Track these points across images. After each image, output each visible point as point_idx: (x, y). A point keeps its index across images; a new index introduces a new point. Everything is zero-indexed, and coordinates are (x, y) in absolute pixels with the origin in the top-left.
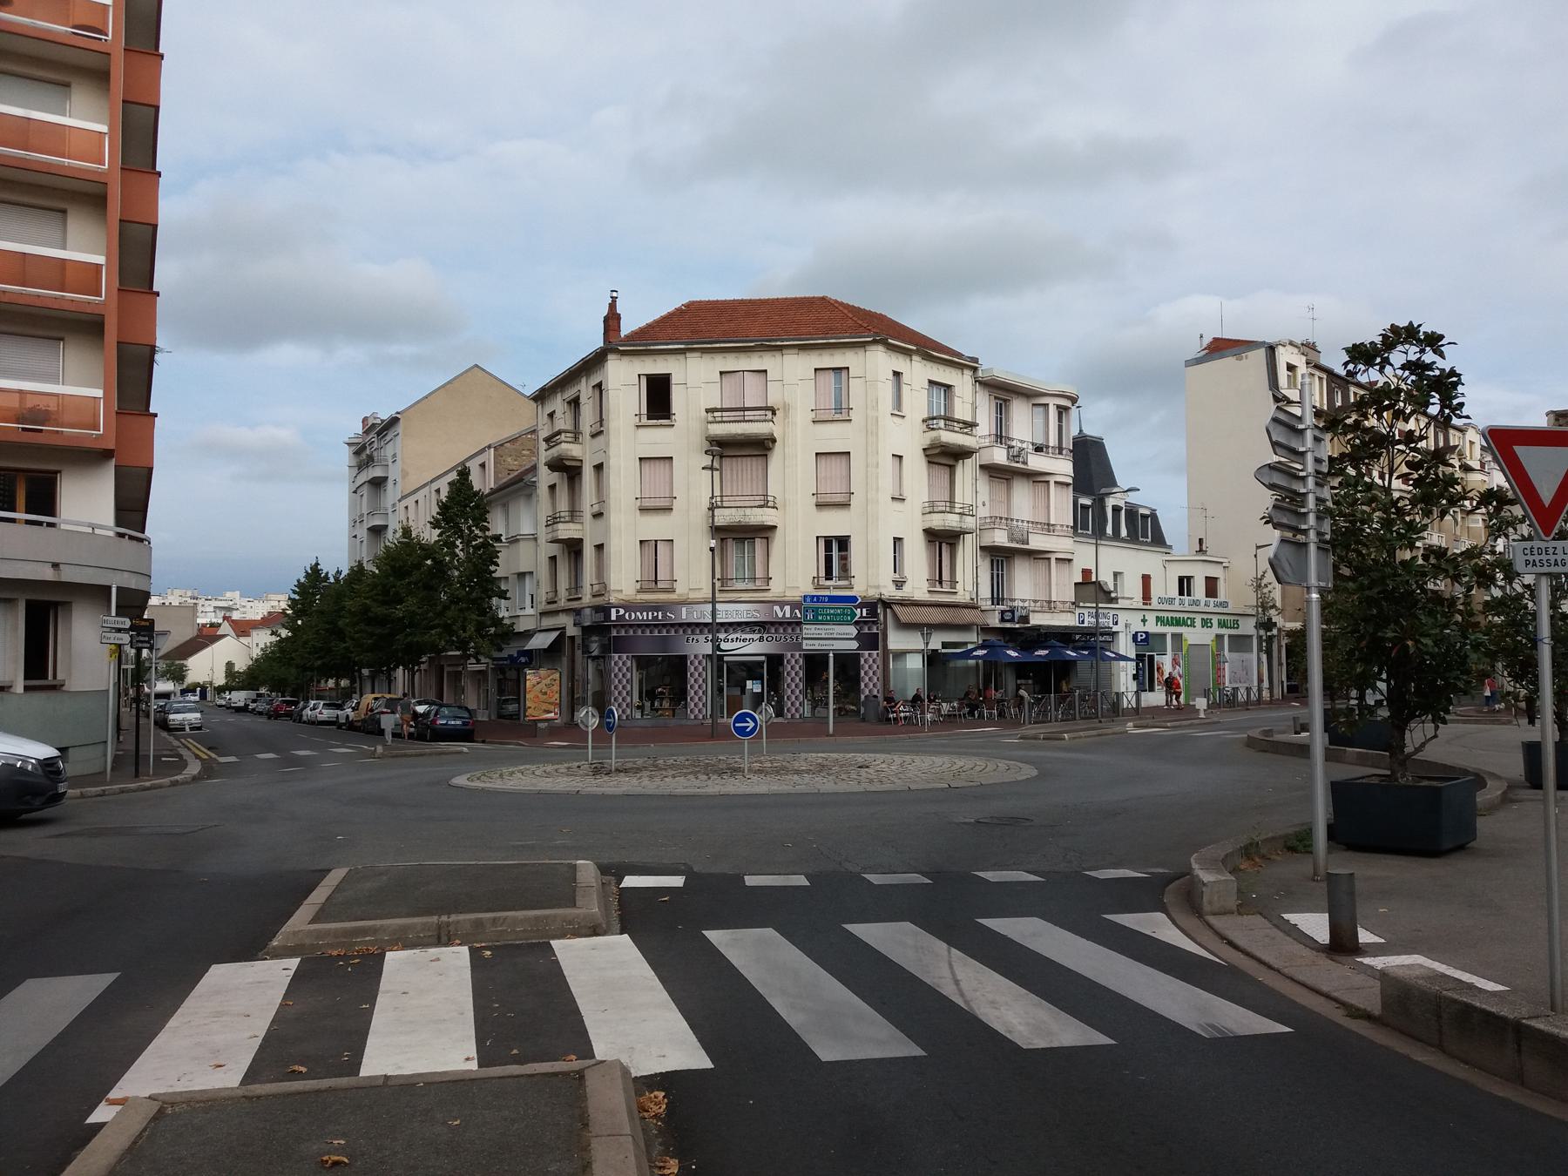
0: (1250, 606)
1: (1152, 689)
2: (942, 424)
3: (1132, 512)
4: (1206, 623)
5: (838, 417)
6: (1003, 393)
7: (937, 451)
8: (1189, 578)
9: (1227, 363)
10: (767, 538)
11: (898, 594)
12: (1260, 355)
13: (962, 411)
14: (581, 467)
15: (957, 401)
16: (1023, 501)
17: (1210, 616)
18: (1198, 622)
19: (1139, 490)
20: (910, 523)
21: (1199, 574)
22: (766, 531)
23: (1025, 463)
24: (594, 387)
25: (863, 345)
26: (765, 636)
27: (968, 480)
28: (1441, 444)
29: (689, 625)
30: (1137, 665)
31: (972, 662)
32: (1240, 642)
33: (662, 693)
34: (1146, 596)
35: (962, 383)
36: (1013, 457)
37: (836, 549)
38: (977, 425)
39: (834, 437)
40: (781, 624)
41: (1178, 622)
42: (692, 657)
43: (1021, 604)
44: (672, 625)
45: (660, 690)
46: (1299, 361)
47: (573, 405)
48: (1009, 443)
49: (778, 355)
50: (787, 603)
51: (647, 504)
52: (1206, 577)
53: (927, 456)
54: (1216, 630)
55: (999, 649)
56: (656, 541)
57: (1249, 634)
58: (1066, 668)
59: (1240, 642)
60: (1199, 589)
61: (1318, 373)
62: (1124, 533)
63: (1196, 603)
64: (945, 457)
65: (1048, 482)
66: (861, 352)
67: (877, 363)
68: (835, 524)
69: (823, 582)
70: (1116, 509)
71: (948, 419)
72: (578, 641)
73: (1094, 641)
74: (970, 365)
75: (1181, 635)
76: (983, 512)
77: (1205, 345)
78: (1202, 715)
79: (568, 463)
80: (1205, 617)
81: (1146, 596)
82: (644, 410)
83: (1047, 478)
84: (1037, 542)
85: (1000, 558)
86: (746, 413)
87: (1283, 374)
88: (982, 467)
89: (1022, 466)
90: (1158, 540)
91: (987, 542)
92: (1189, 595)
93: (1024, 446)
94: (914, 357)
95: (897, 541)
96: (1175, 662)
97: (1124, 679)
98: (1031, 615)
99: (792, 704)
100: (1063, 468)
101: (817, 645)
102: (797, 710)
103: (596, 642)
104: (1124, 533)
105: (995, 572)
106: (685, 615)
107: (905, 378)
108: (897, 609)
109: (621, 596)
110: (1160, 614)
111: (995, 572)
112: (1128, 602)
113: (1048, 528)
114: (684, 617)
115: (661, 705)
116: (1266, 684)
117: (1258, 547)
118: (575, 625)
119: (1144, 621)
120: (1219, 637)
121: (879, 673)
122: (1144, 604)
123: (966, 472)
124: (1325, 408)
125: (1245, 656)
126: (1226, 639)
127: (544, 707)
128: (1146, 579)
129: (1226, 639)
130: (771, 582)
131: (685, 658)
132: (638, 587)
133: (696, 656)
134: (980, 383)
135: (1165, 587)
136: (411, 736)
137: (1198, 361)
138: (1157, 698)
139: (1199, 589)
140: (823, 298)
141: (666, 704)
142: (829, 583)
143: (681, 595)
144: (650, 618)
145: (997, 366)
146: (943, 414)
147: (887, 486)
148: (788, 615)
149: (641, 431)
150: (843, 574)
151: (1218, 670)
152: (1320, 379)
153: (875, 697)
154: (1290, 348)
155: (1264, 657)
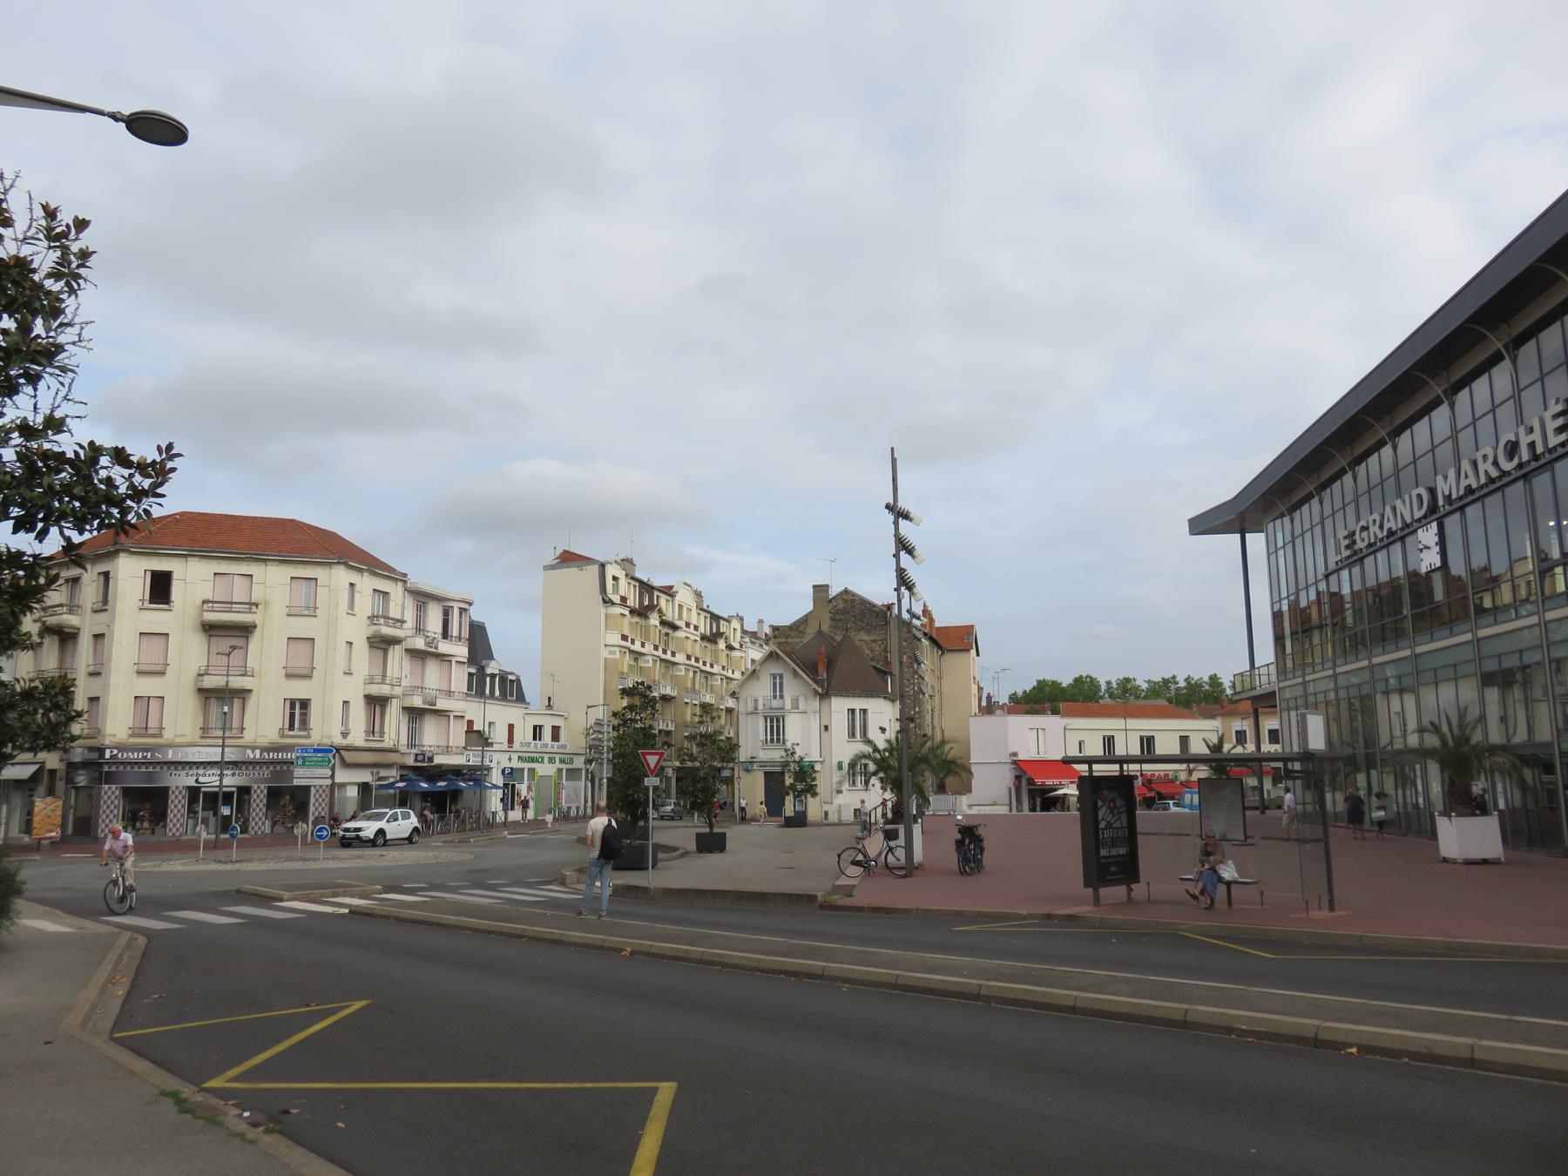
0: (582, 748)
1: (512, 809)
2: (382, 621)
3: (503, 677)
4: (551, 760)
5: (306, 612)
6: (422, 598)
7: (378, 640)
8: (541, 727)
9: (571, 572)
10: (244, 699)
11: (344, 742)
12: (596, 568)
13: (394, 612)
14: (77, 634)
15: (392, 604)
16: (433, 675)
17: (554, 755)
18: (546, 760)
19: (94, 322)
20: (355, 691)
21: (548, 724)
22: (243, 694)
23: (436, 648)
24: (99, 574)
25: (329, 564)
26: (237, 772)
27: (396, 658)
28: (714, 631)
29: (173, 763)
30: (504, 791)
31: (391, 791)
32: (573, 774)
33: (143, 816)
34: (511, 740)
35: (396, 591)
36: (428, 644)
37: (299, 709)
38: (406, 622)
39: (303, 627)
40: (251, 763)
41: (532, 760)
42: (174, 789)
43: (429, 749)
44: (158, 763)
45: (142, 813)
46: (621, 574)
47: (70, 584)
48: (426, 634)
49: (263, 565)
50: (257, 748)
51: (142, 668)
52: (553, 726)
53: (369, 642)
54: (558, 765)
55: (415, 782)
56: (149, 697)
57: (854, 867)
58: (456, 794)
59: (573, 774)
60: (547, 734)
61: (633, 582)
62: (497, 693)
63: (545, 745)
64: (381, 644)
65: (451, 661)
66: (327, 569)
67: (341, 576)
68: (299, 690)
69: (287, 732)
70: (493, 676)
71: (387, 618)
72: (61, 774)
73: (476, 775)
74: (400, 578)
75: (534, 769)
76: (405, 682)
77: (557, 555)
78: (549, 826)
79: (67, 630)
80: (551, 756)
81: (511, 740)
82: (147, 596)
83: (450, 658)
84: (442, 704)
85: (415, 715)
86: (234, 606)
87: (610, 583)
88: (406, 650)
89: (435, 651)
90: (521, 699)
91: (408, 704)
92: (540, 740)
93: (436, 636)
94: (365, 574)
95: (346, 703)
96: (529, 789)
97: (494, 802)
98: (435, 757)
99: (256, 824)
100: (461, 651)
101: (303, 782)
102: (260, 828)
103: (83, 775)
104: (497, 693)
105: (411, 725)
106: (170, 755)
107: (357, 588)
108: (343, 753)
109: (114, 740)
110: (521, 754)
111: (411, 725)
112: (499, 745)
113: (449, 693)
114: (170, 757)
115: (28, 827)
116: (589, 803)
117: (589, 707)
118: (61, 760)
119: (510, 759)
120: (560, 770)
121: (327, 800)
122: (509, 747)
123: (395, 653)
124: (637, 606)
125: (576, 783)
126: (564, 771)
127: (50, 827)
128: (511, 727)
129: (564, 771)
130: (244, 732)
131: (166, 789)
132: (130, 732)
133: (177, 788)
134: (409, 591)
135: (523, 735)
136: (54, 844)
137: (552, 567)
138: (515, 815)
139: (547, 734)
140: (293, 521)
141: (146, 825)
142: (291, 733)
143: (167, 740)
144: (140, 757)
145: (419, 580)
146: (381, 613)
147: (341, 664)
148: (258, 756)
149: (143, 612)
150: (302, 727)
151: (558, 794)
152: (635, 586)
153: (323, 817)
154: (615, 565)
155: (589, 784)
